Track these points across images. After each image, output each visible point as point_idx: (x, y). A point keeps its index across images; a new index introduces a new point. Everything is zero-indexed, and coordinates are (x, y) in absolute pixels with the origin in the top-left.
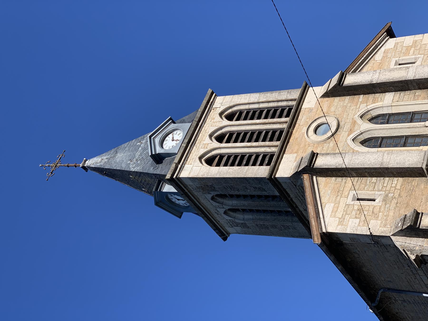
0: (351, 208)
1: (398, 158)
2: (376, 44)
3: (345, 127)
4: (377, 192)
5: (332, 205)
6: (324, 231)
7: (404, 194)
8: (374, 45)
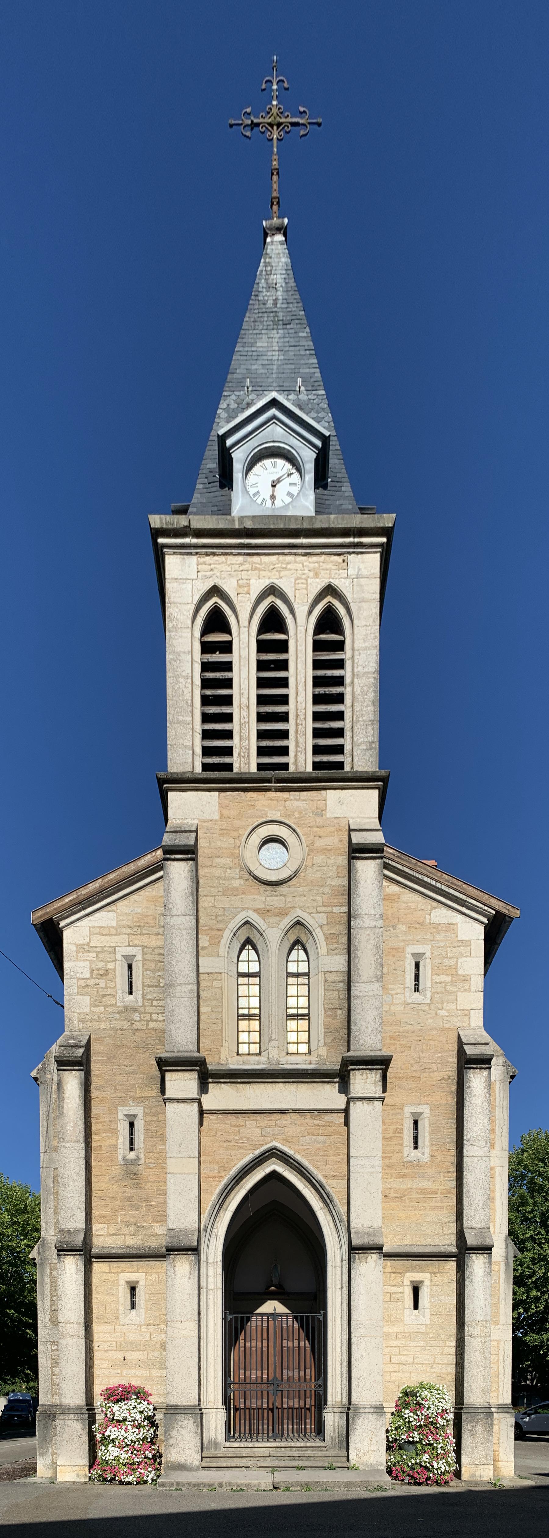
0: (108, 957)
1: (182, 1011)
4: (141, 992)
5: (114, 924)
7: (138, 1037)
8: (464, 897)
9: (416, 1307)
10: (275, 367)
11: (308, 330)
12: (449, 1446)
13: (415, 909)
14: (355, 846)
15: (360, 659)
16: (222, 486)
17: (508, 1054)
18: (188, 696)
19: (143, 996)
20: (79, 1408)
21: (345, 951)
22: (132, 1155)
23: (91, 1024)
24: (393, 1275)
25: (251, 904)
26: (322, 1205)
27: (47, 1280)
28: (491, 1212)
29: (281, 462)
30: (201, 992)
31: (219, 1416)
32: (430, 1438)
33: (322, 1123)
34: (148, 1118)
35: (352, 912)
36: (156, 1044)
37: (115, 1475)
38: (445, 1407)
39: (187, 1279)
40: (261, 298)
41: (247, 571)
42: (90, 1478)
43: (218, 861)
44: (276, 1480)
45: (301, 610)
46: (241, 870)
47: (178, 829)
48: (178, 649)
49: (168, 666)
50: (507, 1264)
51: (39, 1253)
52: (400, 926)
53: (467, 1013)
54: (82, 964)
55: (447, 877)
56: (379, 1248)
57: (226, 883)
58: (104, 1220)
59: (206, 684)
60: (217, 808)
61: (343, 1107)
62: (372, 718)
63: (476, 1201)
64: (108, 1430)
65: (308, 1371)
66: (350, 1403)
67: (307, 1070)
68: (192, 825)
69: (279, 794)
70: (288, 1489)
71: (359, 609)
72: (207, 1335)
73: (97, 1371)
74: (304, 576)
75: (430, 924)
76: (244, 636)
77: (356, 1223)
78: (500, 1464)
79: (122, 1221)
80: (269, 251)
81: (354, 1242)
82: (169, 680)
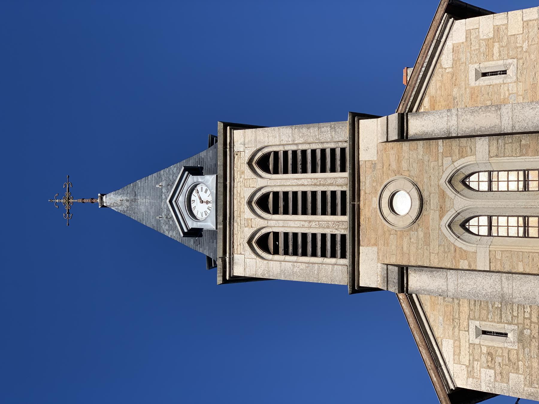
0: (477, 351)
1: (524, 289)
2: (436, 38)
3: (432, 201)
4: (506, 325)
5: (451, 342)
13: (442, 81)
14: (400, 137)
18: (303, 266)
19: (510, 324)
21: (473, 139)
23: (534, 376)
25: (437, 221)
30: (506, 270)
35: (445, 136)
46: (411, 229)
47: (386, 279)
53: (526, 24)
54: (483, 375)
60: (370, 248)
68: (382, 268)
69: (361, 199)
71: (260, 142)
75: (453, 67)
82: (295, 279)
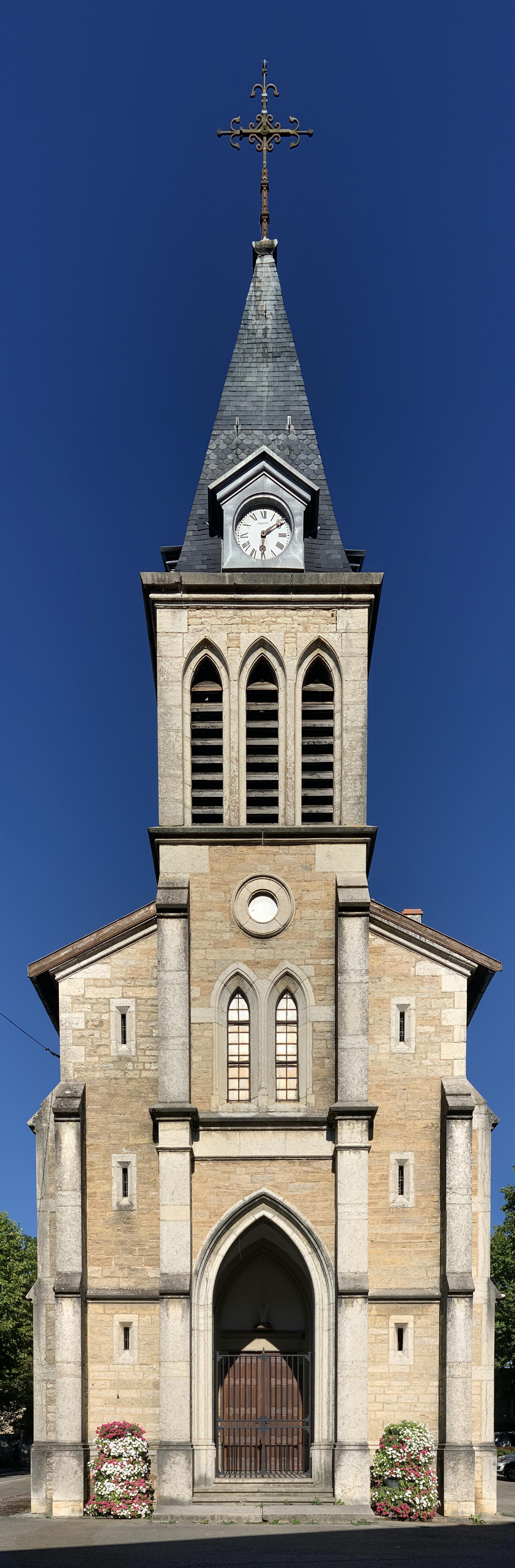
0: (103, 1009)
1: (175, 1062)
3: (266, 951)
5: (108, 976)
6: (58, 976)
7: (132, 1086)
8: (448, 951)
9: (400, 1348)
10: (265, 404)
11: (297, 363)
12: (431, 1483)
13: (400, 962)
15: (349, 713)
16: (212, 535)
17: (489, 1103)
18: (178, 750)
20: (74, 1445)
21: (333, 1002)
22: (125, 1201)
23: (86, 1074)
24: (378, 1318)
25: (242, 957)
26: (310, 1250)
27: (43, 1320)
28: (474, 1257)
29: (270, 513)
30: (192, 1042)
31: (210, 1452)
32: (413, 1475)
33: (310, 1169)
34: (141, 1165)
35: (339, 967)
36: (148, 1093)
37: (110, 1510)
38: (427, 1445)
39: (179, 1321)
40: (250, 327)
41: (237, 624)
42: (85, 1513)
43: (209, 914)
44: (265, 1514)
45: (291, 663)
47: (171, 886)
48: (169, 703)
49: (160, 720)
50: (489, 1307)
51: (35, 1294)
52: (386, 978)
53: (450, 1063)
54: (77, 1015)
55: (431, 931)
56: (364, 1293)
57: (217, 936)
58: (98, 1262)
59: (196, 734)
60: (207, 862)
61: (331, 1154)
62: (360, 773)
63: (459, 1247)
64: (105, 1466)
65: (296, 1409)
66: (336, 1441)
67: (296, 1118)
69: (268, 848)
70: (276, 1522)
71: (348, 663)
72: (198, 1375)
73: (91, 1409)
74: (293, 630)
75: (415, 976)
76: (234, 689)
77: (343, 1268)
78: (483, 1502)
79: (116, 1264)
80: (258, 274)
81: (341, 1287)
82: (160, 734)
